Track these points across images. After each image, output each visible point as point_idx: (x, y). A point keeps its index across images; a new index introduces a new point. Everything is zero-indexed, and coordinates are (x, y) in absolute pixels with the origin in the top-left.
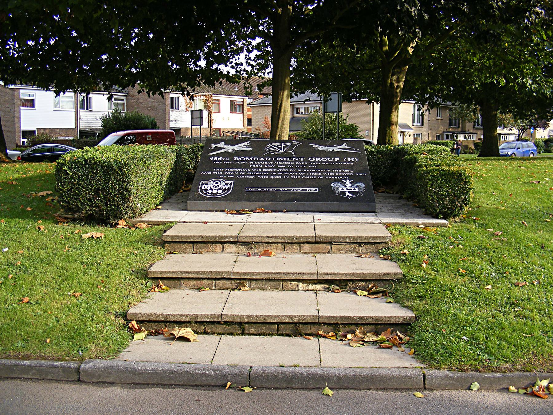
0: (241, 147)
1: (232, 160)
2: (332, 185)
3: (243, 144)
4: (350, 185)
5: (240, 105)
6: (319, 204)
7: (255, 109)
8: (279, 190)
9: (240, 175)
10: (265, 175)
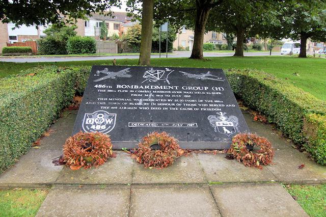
1: (114, 88)
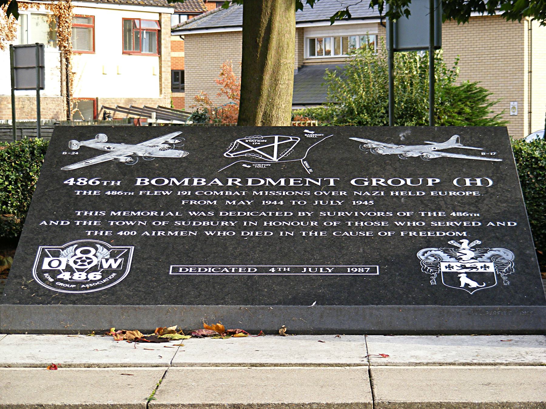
0: (157, 148)
1: (130, 185)
2: (419, 254)
3: (162, 139)
4: (473, 254)
5: (150, 32)
6: (384, 312)
7: (194, 42)
8: (267, 270)
9: (153, 228)
10: (224, 228)
